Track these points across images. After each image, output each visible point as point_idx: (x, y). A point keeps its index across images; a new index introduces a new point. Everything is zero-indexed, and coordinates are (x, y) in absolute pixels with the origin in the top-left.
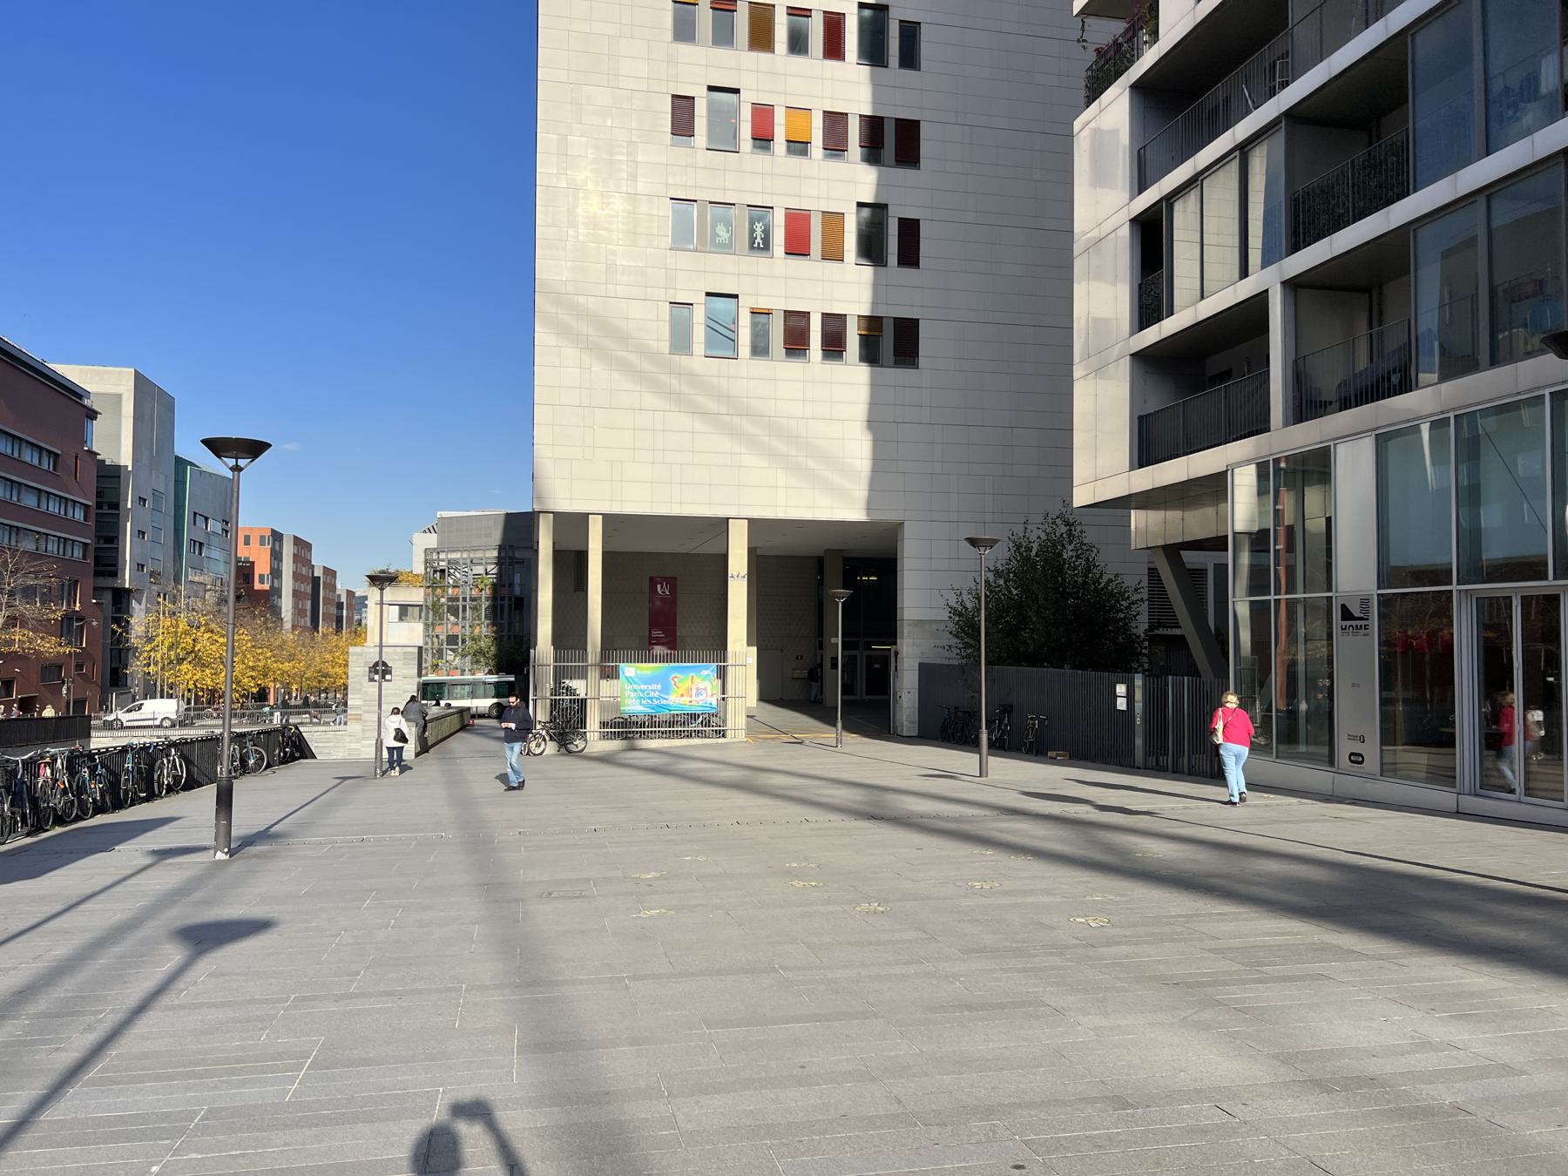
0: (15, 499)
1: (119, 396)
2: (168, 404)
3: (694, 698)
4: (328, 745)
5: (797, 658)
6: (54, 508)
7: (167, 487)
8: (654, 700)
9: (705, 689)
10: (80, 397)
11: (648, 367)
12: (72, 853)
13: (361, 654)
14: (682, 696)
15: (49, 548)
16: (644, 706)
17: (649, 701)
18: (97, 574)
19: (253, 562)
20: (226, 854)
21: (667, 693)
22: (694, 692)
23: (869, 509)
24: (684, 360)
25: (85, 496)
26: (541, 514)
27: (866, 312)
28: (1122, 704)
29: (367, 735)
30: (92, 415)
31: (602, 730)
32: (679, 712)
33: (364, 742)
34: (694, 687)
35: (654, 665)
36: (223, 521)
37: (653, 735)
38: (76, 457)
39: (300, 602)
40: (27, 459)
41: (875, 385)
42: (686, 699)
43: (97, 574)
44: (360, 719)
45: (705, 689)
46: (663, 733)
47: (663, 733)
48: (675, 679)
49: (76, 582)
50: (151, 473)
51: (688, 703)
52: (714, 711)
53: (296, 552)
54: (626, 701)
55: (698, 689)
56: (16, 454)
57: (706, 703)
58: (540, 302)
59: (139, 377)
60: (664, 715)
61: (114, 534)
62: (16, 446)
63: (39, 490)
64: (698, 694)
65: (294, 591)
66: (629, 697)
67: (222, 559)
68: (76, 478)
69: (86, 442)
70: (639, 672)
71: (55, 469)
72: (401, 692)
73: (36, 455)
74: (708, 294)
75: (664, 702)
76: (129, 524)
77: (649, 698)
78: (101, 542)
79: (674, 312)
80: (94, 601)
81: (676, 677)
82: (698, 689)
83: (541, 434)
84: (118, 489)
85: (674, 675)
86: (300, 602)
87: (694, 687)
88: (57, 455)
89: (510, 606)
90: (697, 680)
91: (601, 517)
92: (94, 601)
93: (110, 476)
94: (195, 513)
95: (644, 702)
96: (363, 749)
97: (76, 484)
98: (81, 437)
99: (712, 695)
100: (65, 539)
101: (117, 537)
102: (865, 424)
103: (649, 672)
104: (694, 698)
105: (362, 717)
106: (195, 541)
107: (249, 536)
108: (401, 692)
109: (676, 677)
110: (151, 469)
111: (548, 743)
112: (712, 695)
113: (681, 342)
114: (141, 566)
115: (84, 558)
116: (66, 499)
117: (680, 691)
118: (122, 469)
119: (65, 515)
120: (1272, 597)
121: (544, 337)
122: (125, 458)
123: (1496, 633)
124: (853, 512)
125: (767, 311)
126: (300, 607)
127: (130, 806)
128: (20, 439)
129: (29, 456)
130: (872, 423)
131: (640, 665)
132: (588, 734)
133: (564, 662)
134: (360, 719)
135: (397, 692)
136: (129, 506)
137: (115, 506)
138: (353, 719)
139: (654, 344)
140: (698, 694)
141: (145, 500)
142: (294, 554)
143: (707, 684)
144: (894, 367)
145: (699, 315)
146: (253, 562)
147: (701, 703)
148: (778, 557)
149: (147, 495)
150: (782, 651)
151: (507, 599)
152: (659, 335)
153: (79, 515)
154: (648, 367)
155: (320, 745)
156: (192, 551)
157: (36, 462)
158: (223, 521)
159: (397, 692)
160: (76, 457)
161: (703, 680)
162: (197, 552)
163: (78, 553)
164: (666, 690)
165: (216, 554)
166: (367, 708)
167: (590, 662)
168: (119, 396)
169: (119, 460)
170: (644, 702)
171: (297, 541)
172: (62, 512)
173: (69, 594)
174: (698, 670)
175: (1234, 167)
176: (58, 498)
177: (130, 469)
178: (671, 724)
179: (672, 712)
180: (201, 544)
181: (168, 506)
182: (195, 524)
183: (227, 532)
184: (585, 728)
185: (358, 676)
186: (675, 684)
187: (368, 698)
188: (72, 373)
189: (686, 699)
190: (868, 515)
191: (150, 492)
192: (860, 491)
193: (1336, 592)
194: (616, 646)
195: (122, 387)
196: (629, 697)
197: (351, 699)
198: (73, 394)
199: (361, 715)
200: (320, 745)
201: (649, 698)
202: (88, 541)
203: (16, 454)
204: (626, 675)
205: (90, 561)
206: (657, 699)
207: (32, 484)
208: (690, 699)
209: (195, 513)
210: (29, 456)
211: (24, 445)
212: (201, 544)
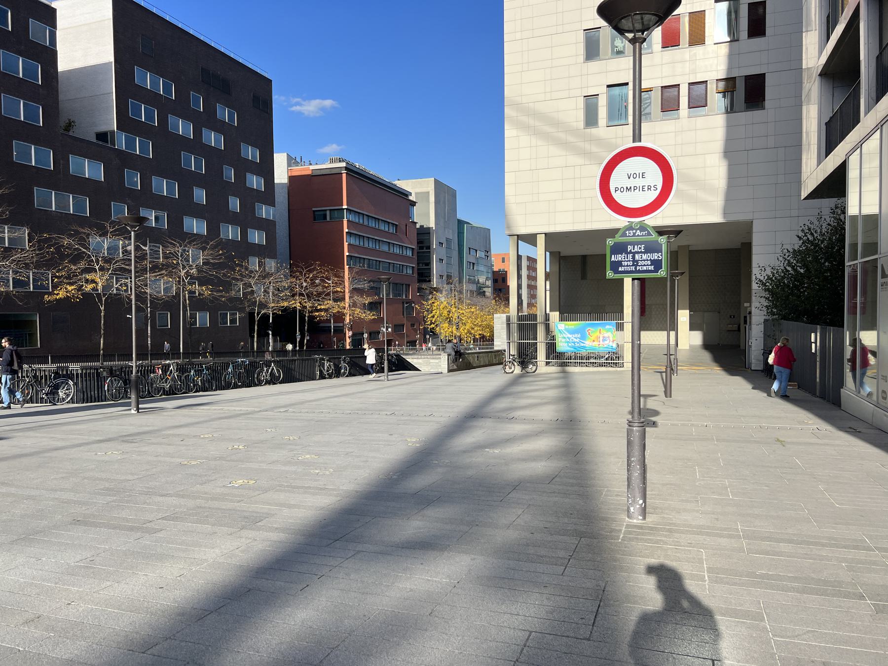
0: (377, 247)
1: (428, 193)
2: (453, 194)
3: (601, 343)
5: (731, 317)
6: (397, 251)
7: (453, 236)
8: (576, 343)
9: (609, 337)
10: (407, 196)
11: (571, 139)
13: (500, 318)
14: (594, 341)
15: (408, 272)
16: (570, 347)
17: (573, 344)
18: (420, 281)
19: (507, 271)
20: (135, 411)
21: (585, 340)
22: (601, 339)
23: (725, 213)
24: (593, 131)
25: (412, 244)
26: (538, 235)
27: (722, 75)
28: (813, 351)
30: (413, 204)
31: (548, 361)
32: (592, 351)
34: (601, 336)
35: (576, 322)
36: (485, 251)
37: (570, 364)
38: (406, 225)
39: (532, 291)
40: (382, 228)
41: (730, 127)
42: (596, 343)
43: (420, 281)
45: (609, 337)
46: (584, 363)
47: (609, 364)
48: (589, 331)
49: (409, 285)
50: (445, 230)
51: (597, 346)
52: (614, 351)
53: (528, 265)
54: (560, 343)
55: (604, 337)
56: (377, 227)
57: (609, 346)
58: (508, 111)
59: (437, 182)
60: (584, 352)
61: (428, 261)
62: (377, 223)
63: (389, 243)
64: (603, 340)
65: (528, 285)
66: (561, 341)
67: (485, 271)
68: (406, 235)
69: (411, 218)
70: (567, 327)
71: (396, 232)
73: (387, 226)
74: (609, 86)
75: (582, 345)
76: (434, 256)
77: (573, 342)
78: (424, 265)
79: (665, 95)
80: (418, 294)
81: (590, 330)
82: (604, 337)
83: (509, 190)
84: (429, 239)
85: (589, 329)
86: (532, 291)
87: (601, 336)
88: (396, 225)
90: (603, 331)
91: (544, 235)
92: (418, 294)
93: (424, 234)
95: (570, 345)
97: (406, 239)
98: (408, 215)
99: (613, 341)
100: (403, 265)
101: (430, 263)
102: (722, 154)
103: (573, 327)
104: (601, 343)
106: (470, 263)
107: (504, 258)
109: (590, 330)
110: (445, 228)
111: (516, 367)
112: (613, 341)
113: (591, 119)
114: (441, 276)
115: (413, 274)
116: (402, 246)
117: (593, 338)
118: (431, 230)
119: (402, 254)
120: (860, 260)
121: (510, 132)
122: (432, 224)
124: (715, 217)
125: (649, 90)
126: (532, 293)
127: (231, 389)
128: (379, 219)
129: (382, 227)
130: (729, 152)
131: (567, 322)
132: (538, 362)
133: (521, 321)
136: (434, 247)
137: (429, 247)
139: (575, 124)
140: (603, 340)
141: (442, 244)
142: (527, 266)
143: (609, 334)
144: (745, 111)
145: (602, 102)
146: (507, 271)
147: (605, 346)
148: (717, 251)
149: (444, 241)
150: (719, 312)
152: (578, 116)
153: (409, 253)
154: (571, 139)
156: (469, 267)
157: (387, 229)
158: (485, 251)
160: (406, 225)
161: (607, 332)
162: (471, 268)
163: (410, 271)
164: (583, 337)
165: (482, 268)
167: (538, 321)
168: (428, 193)
169: (429, 224)
170: (570, 345)
171: (529, 258)
172: (401, 253)
173: (406, 291)
174: (604, 325)
176: (398, 246)
177: (434, 229)
178: (588, 358)
179: (588, 351)
180: (473, 264)
181: (455, 246)
182: (470, 254)
183: (488, 257)
184: (536, 359)
186: (589, 334)
188: (403, 184)
189: (596, 343)
190: (724, 217)
191: (445, 239)
192: (718, 201)
193: (880, 254)
194: (607, 311)
195: (429, 188)
196: (561, 341)
198: (404, 195)
201: (573, 342)
202: (414, 266)
203: (377, 227)
204: (559, 328)
205: (416, 275)
206: (578, 343)
207: (385, 240)
208: (598, 343)
209: (470, 248)
210: (382, 227)
211: (380, 222)
212: (473, 264)
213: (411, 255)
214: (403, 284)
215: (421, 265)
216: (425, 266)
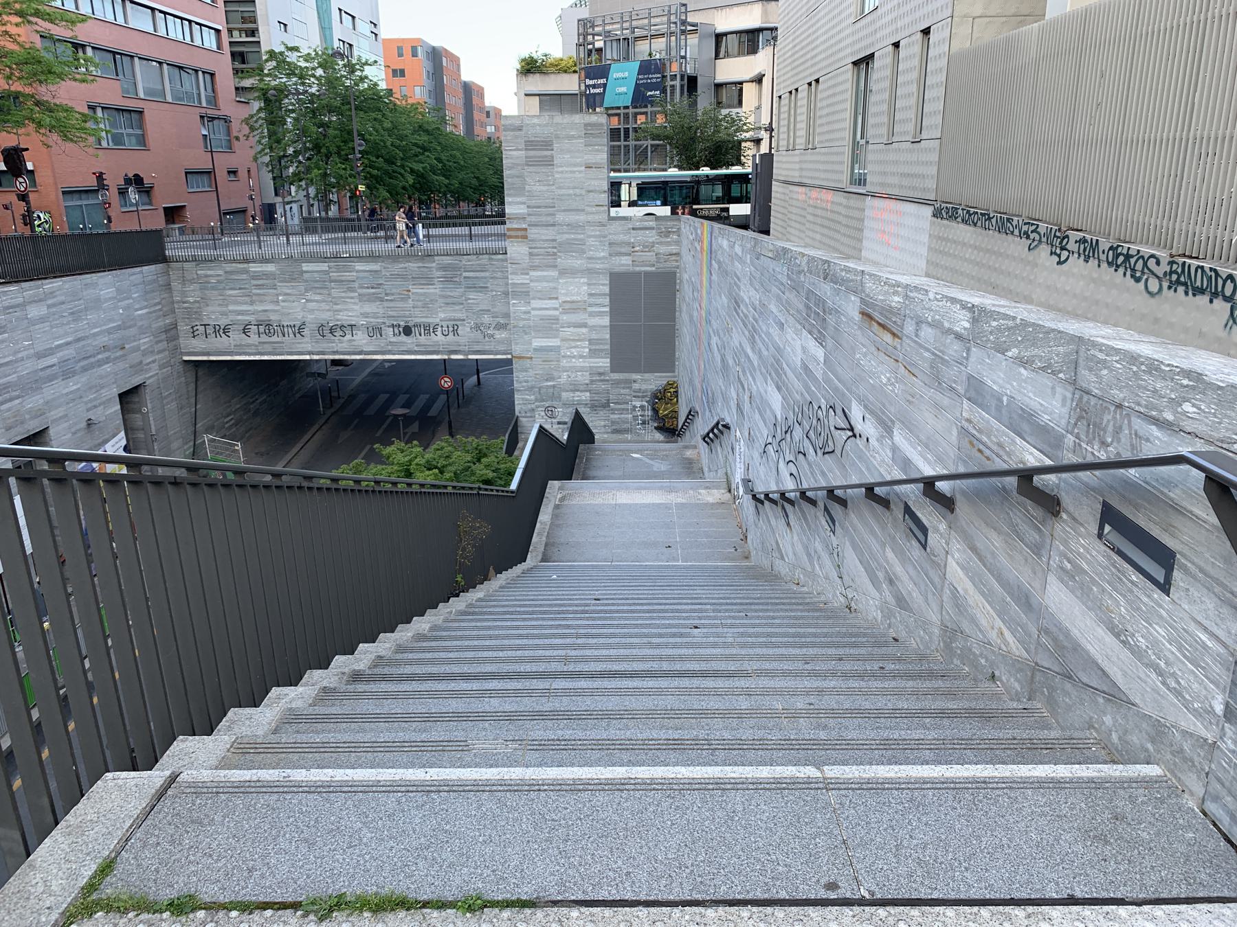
4: (483, 274)
12: (841, 659)
29: (537, 262)
33: (532, 273)
44: (526, 237)
72: (583, 192)
78: (244, 35)
89: (682, 86)
94: (340, 10)
96: (532, 284)
105: (531, 236)
108: (583, 192)
119: (192, 41)
123: (851, 401)
134: (526, 237)
135: (578, 191)
138: (517, 237)
151: (678, 77)
153: (210, 41)
155: (471, 274)
159: (578, 191)
166: (533, 219)
175: (108, 890)
185: (518, 165)
187: (533, 202)
197: (510, 203)
199: (525, 230)
200: (471, 274)
213: (214, 47)
214: (196, 71)
215: (236, 33)
216: (247, 36)
